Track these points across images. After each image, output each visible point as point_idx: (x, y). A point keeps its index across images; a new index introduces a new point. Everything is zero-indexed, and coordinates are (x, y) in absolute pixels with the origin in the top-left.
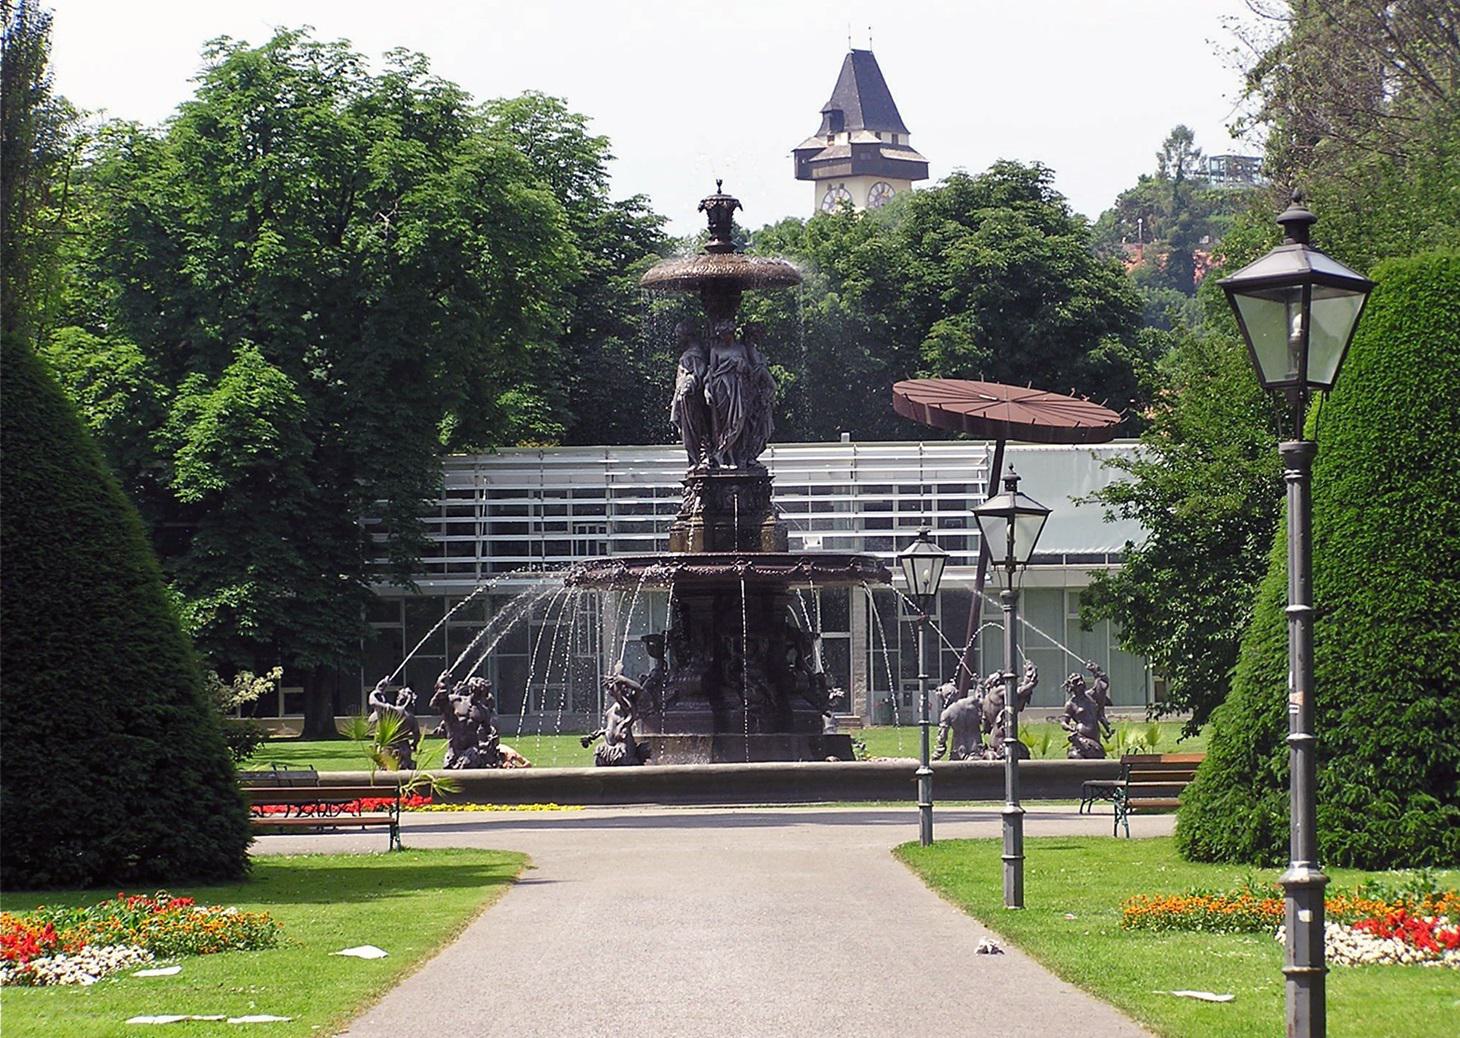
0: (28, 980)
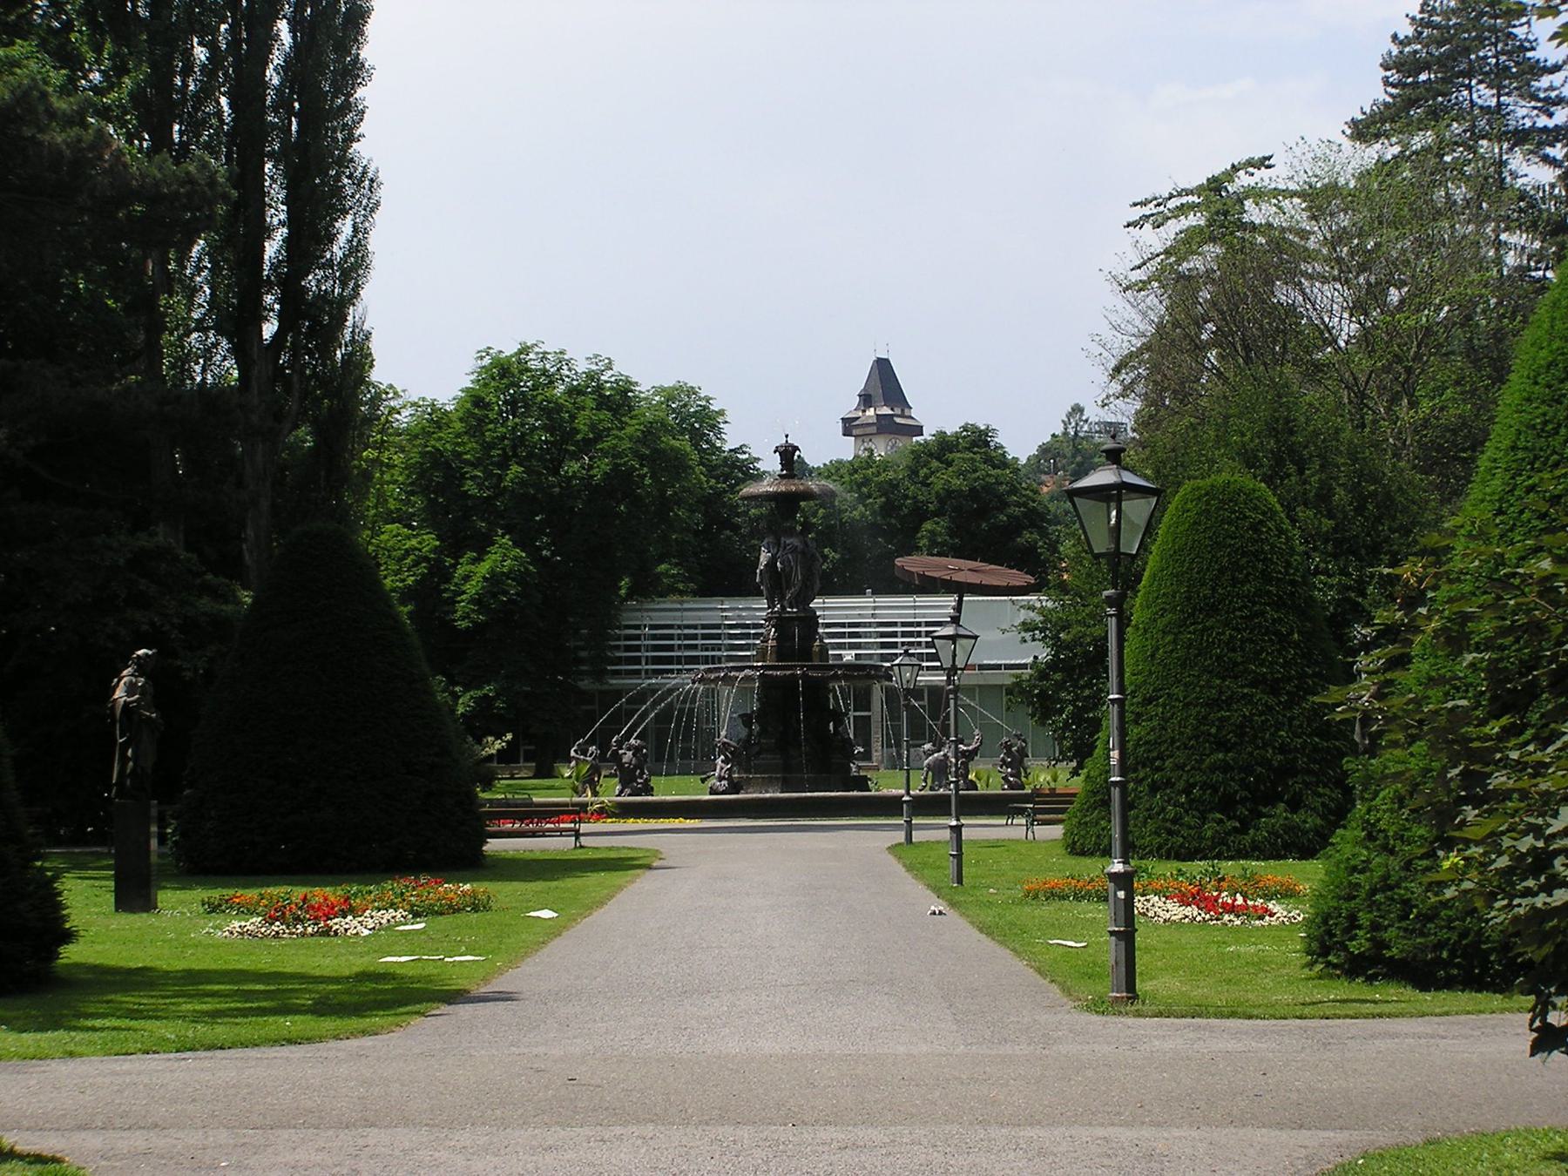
0: (326, 932)
